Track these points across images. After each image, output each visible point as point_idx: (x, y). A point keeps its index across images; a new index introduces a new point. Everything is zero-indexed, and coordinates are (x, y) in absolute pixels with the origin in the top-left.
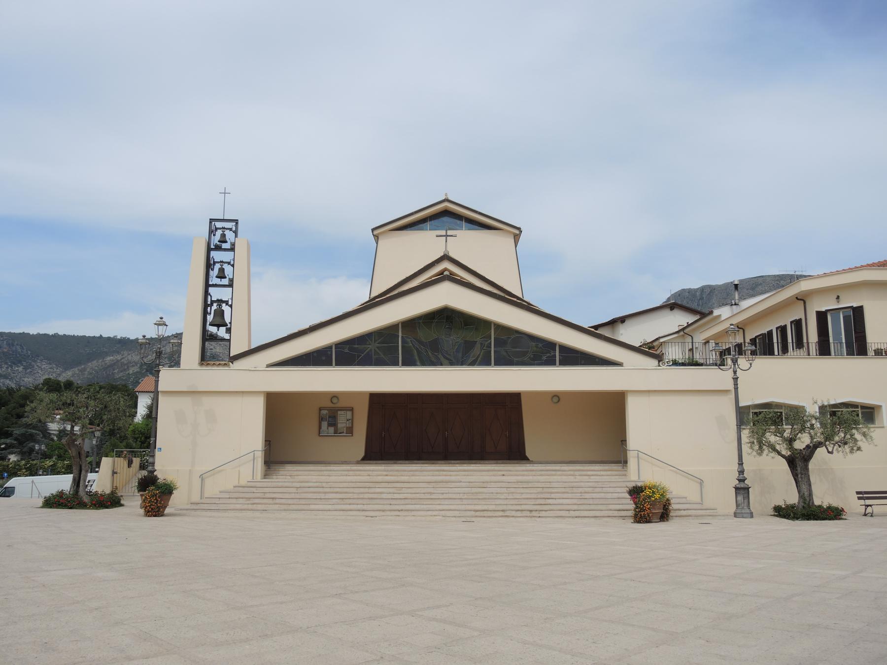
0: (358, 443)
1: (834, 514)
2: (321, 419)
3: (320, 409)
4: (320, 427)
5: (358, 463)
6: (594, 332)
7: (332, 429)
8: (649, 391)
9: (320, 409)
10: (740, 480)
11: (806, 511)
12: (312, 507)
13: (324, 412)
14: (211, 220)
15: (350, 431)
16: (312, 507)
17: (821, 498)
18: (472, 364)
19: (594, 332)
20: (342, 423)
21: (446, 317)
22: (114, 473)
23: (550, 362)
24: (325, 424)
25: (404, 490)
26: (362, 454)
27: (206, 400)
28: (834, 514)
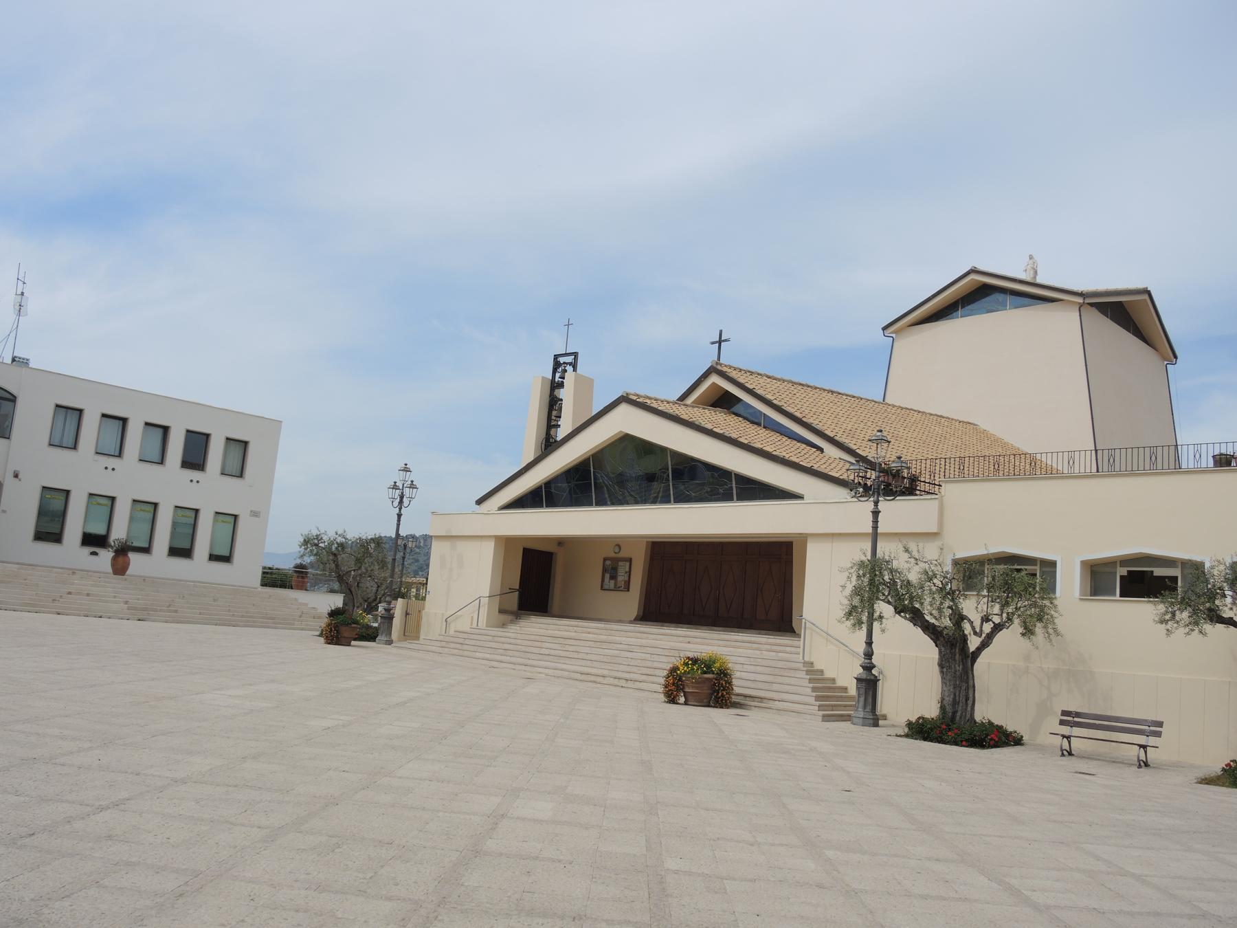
0: (632, 601)
1: (993, 737)
2: (605, 571)
3: (605, 560)
4: (603, 581)
5: (631, 622)
6: (549, 445)
7: (613, 582)
8: (840, 534)
9: (605, 560)
10: (864, 668)
11: (956, 725)
12: (478, 655)
13: (608, 563)
14: (556, 357)
15: (627, 587)
16: (478, 655)
17: (985, 711)
18: (654, 502)
19: (549, 445)
20: (622, 578)
21: (627, 444)
22: (407, 614)
23: (727, 497)
24: (607, 576)
25: (567, 648)
26: (634, 614)
27: (461, 545)
28: (993, 737)
